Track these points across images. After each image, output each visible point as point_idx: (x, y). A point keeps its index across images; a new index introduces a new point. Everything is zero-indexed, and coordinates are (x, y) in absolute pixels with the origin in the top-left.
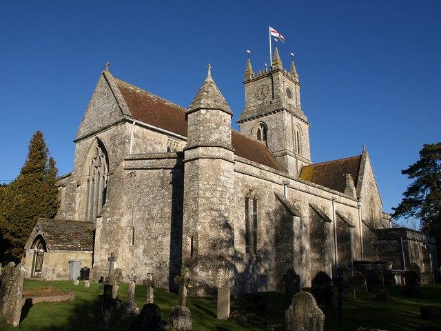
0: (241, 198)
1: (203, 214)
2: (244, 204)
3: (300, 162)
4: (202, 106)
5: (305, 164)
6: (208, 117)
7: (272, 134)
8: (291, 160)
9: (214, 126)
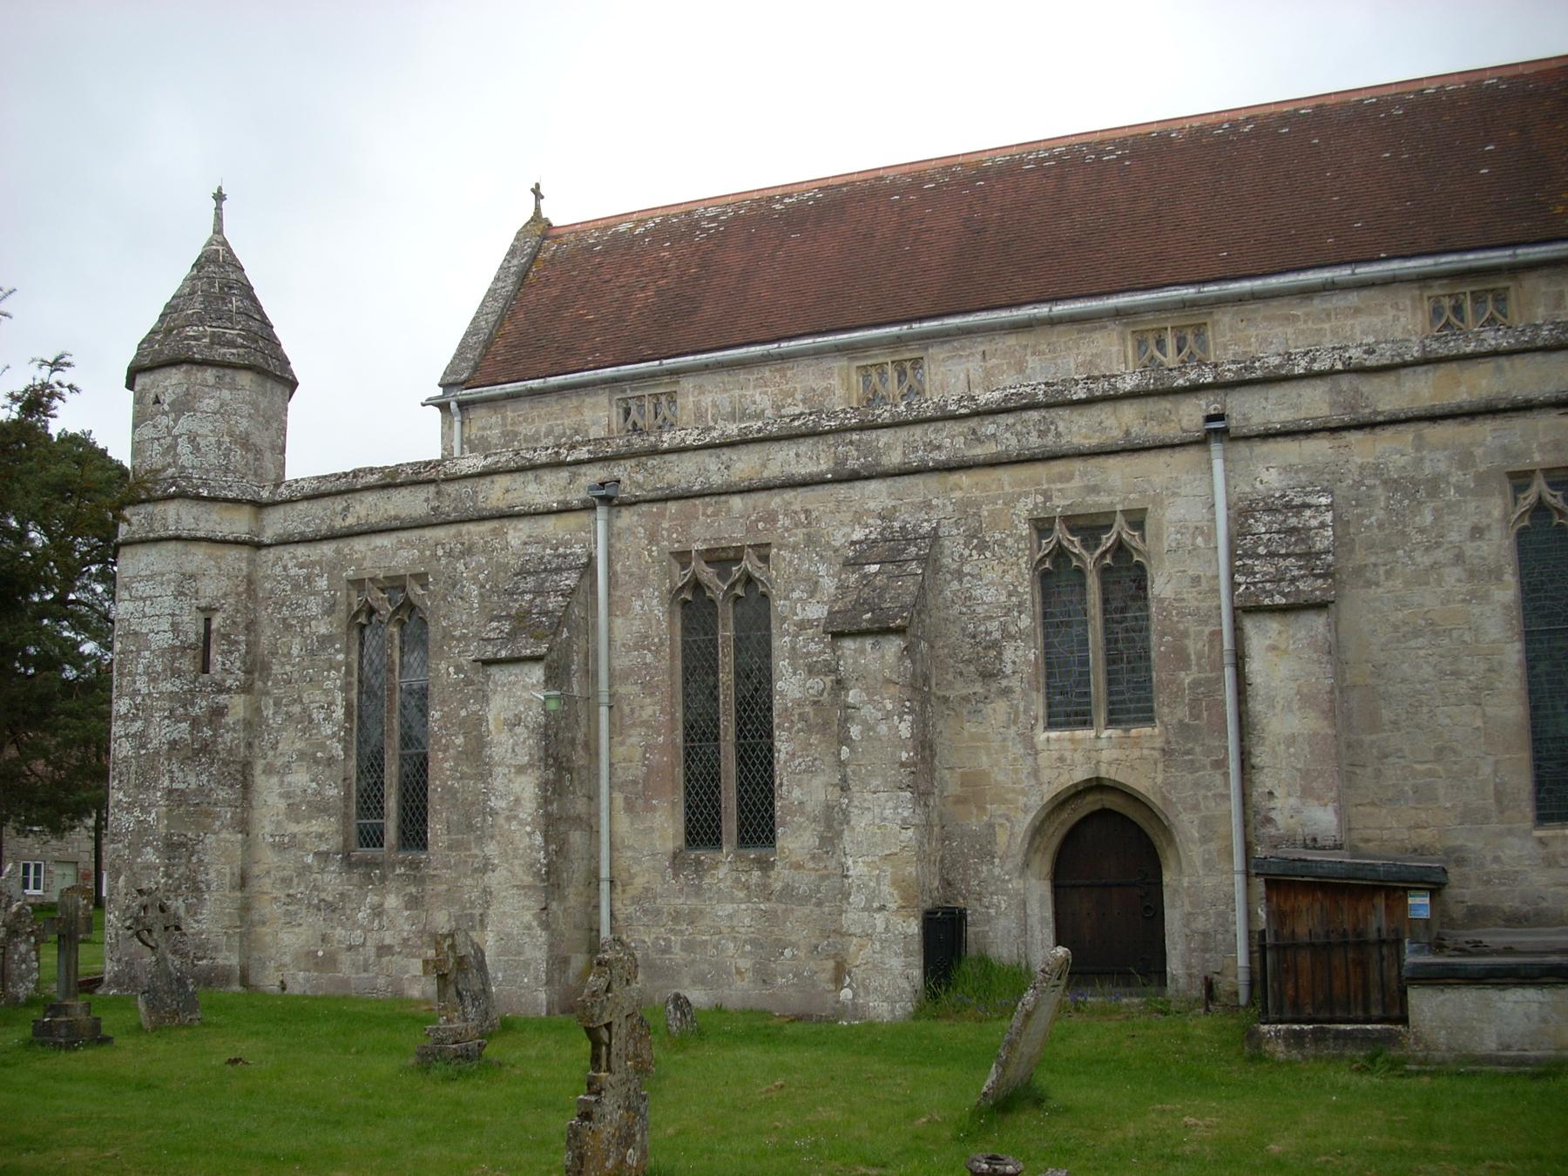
0: (325, 641)
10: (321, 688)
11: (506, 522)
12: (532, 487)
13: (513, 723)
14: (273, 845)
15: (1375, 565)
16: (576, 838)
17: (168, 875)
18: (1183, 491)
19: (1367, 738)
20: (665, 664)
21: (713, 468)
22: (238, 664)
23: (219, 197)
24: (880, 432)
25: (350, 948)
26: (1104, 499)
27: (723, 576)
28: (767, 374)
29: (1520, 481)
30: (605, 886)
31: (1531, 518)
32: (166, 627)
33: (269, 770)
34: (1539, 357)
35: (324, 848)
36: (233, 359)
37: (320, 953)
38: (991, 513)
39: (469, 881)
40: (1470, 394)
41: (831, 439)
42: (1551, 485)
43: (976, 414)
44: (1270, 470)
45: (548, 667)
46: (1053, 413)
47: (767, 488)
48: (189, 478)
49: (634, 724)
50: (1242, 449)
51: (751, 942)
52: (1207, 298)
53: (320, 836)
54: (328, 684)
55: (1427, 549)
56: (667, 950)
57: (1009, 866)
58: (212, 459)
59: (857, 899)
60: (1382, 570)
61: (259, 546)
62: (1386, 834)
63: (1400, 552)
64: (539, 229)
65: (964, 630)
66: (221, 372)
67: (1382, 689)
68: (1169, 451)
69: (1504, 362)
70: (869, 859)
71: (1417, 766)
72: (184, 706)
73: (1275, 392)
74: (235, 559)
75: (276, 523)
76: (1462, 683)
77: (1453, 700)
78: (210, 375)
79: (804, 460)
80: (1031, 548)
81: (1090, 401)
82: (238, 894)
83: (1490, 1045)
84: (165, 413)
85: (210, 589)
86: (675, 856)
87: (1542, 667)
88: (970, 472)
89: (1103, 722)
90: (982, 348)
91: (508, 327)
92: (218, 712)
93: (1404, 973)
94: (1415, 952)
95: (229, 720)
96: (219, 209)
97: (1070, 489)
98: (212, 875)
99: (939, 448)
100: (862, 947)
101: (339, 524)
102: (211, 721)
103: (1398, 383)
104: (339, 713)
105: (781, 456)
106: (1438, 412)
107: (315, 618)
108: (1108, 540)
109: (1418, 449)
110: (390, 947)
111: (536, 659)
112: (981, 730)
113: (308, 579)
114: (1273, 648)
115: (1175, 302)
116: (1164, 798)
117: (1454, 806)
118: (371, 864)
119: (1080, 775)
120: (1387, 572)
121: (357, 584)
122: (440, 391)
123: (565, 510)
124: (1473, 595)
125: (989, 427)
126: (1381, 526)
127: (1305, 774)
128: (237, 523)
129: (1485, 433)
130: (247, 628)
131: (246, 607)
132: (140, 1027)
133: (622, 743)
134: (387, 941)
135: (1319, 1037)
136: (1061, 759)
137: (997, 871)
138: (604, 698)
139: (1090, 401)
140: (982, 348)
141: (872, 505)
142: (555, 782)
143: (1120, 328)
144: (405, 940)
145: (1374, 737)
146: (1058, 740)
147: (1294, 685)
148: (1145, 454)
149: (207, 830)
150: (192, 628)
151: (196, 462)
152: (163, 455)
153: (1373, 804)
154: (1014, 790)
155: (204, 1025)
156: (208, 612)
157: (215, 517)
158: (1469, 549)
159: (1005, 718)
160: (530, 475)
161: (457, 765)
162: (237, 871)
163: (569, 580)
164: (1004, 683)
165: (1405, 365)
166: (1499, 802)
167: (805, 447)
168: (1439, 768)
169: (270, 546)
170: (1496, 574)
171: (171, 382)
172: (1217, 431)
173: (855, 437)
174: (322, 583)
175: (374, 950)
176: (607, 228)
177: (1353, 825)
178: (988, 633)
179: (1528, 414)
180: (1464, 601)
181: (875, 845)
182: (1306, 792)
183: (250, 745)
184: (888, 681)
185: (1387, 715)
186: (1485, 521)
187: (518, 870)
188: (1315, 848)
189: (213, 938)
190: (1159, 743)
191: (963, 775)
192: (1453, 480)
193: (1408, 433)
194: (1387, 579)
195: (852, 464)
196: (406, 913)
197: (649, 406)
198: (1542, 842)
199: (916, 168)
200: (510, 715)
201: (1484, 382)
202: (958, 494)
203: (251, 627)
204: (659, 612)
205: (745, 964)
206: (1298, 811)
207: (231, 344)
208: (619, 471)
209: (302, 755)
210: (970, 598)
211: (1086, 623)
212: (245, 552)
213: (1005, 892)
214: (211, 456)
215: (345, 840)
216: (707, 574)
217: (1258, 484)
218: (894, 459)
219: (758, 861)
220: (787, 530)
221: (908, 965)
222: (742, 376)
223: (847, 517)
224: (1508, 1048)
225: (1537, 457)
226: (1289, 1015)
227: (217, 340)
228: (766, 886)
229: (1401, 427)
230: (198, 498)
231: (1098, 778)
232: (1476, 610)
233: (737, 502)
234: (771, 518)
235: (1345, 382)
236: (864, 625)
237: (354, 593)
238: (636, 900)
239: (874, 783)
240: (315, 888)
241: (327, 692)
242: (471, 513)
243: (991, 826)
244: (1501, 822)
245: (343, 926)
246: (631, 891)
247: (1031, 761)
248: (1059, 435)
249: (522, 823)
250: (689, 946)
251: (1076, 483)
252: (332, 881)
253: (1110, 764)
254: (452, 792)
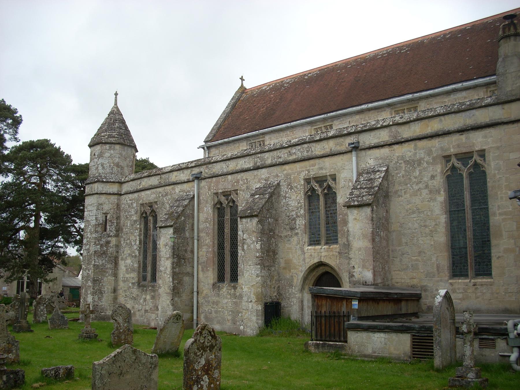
0: (135, 221)
11: (175, 186)
12: (182, 175)
13: (166, 245)
14: (122, 280)
15: (401, 190)
16: (186, 279)
17: (93, 289)
18: (346, 168)
19: (398, 248)
20: (212, 227)
21: (224, 167)
22: (114, 229)
23: (116, 94)
24: (265, 153)
25: (139, 311)
26: (324, 171)
27: (465, 165)
28: (289, 133)
29: (448, 159)
30: (195, 294)
31: (451, 171)
32: (94, 219)
33: (122, 259)
34: (453, 115)
35: (134, 281)
36: (114, 142)
38: (294, 177)
40: (431, 130)
41: (253, 157)
42: (458, 160)
43: (290, 146)
44: (371, 159)
45: (175, 229)
46: (311, 144)
47: (237, 172)
48: (101, 176)
49: (204, 245)
50: (363, 152)
51: (231, 311)
52: (417, 98)
53: (133, 278)
54: (135, 234)
55: (417, 184)
56: (211, 313)
57: (297, 289)
58: (108, 170)
59: (245, 299)
60: (403, 191)
61: (121, 195)
62: (403, 281)
63: (409, 185)
64: (242, 90)
65: (286, 214)
66: (111, 145)
67: (402, 232)
68: (342, 155)
69: (442, 118)
70: (248, 286)
71: (413, 258)
72: (99, 241)
73: (373, 133)
74: (114, 199)
75: (126, 188)
76: (427, 229)
77: (424, 235)
78: (107, 146)
79: (246, 163)
80: (304, 188)
81: (321, 140)
82: (113, 294)
83: (369, 351)
84: (96, 158)
85: (106, 208)
86: (213, 285)
87: (455, 223)
88: (288, 165)
89: (323, 243)
90: (349, 120)
91: (226, 122)
92: (108, 242)
93: (345, 327)
94: (353, 319)
95: (111, 245)
96: (116, 98)
97: (315, 169)
98: (106, 289)
99: (280, 157)
100: (246, 313)
101: (139, 188)
102: (106, 245)
103: (409, 128)
104: (138, 243)
105: (241, 163)
106: (420, 137)
107: (133, 215)
108: (325, 184)
109: (415, 150)
110: (147, 310)
111: (171, 226)
112: (290, 246)
113: (132, 204)
114: (355, 219)
115: (405, 100)
116: (339, 268)
117: (424, 272)
118: (144, 286)
119: (316, 260)
120: (405, 192)
121: (142, 205)
122: (204, 144)
123: (188, 181)
124: (431, 199)
125: (293, 150)
126: (403, 177)
127: (363, 260)
128: (114, 188)
129: (436, 143)
130: (117, 218)
131: (117, 212)
132: (49, 329)
133: (201, 251)
135: (323, 346)
136: (311, 255)
137: (293, 291)
138: (196, 237)
139: (321, 140)
140: (349, 120)
141: (263, 176)
142: (177, 262)
143: (390, 110)
144: (151, 308)
145: (399, 248)
146: (310, 249)
147: (361, 231)
148: (336, 156)
149: (104, 276)
150: (101, 218)
151: (103, 172)
152: (95, 170)
153: (399, 270)
154: (298, 265)
155: (69, 329)
156: (106, 214)
157: (108, 187)
158: (430, 183)
159: (296, 242)
160: (181, 171)
162: (113, 288)
163: (186, 203)
164: (296, 231)
165: (411, 121)
166: (438, 270)
167: (247, 159)
168: (419, 258)
169: (123, 195)
170: (438, 192)
171: (98, 148)
172: (356, 148)
173: (259, 155)
174: (135, 205)
176: (260, 88)
177: (393, 277)
178: (292, 216)
179: (450, 135)
180: (428, 201)
181: (250, 282)
182: (364, 267)
183: (117, 252)
184: (254, 231)
185: (404, 240)
186: (435, 173)
187: (166, 288)
188: (366, 285)
189: (106, 307)
190: (338, 250)
191: (285, 260)
192: (425, 160)
193: (412, 144)
194: (405, 194)
195: (258, 164)
197: (258, 145)
198: (451, 284)
199: (347, 60)
200: (165, 243)
201: (436, 125)
202: (285, 172)
203: (118, 218)
204: (211, 211)
205: (229, 318)
206: (361, 273)
207: (114, 137)
208: (202, 169)
209: (129, 255)
210: (288, 205)
211: (319, 212)
212: (116, 197)
213: (296, 297)
214: (108, 170)
215: (139, 279)
216: (458, 164)
217: (367, 165)
218: (269, 162)
219: (233, 287)
220: (242, 185)
221: (257, 319)
222: (282, 134)
223: (257, 180)
224: (375, 352)
225: (452, 150)
226: (324, 339)
227: (110, 136)
228: (235, 294)
229: (410, 143)
230: (103, 182)
231: (321, 262)
232: (432, 204)
233: (229, 177)
234: (238, 182)
235: (394, 129)
236: (247, 214)
237: (142, 208)
238: (204, 298)
239: (250, 263)
240: (132, 293)
241: (135, 236)
242: (168, 184)
243: (292, 276)
244: (438, 277)
245: (137, 304)
246: (203, 295)
247: (301, 255)
248: (312, 151)
249: (167, 275)
250: (216, 312)
251: (317, 167)
252: (135, 291)
253: (324, 257)
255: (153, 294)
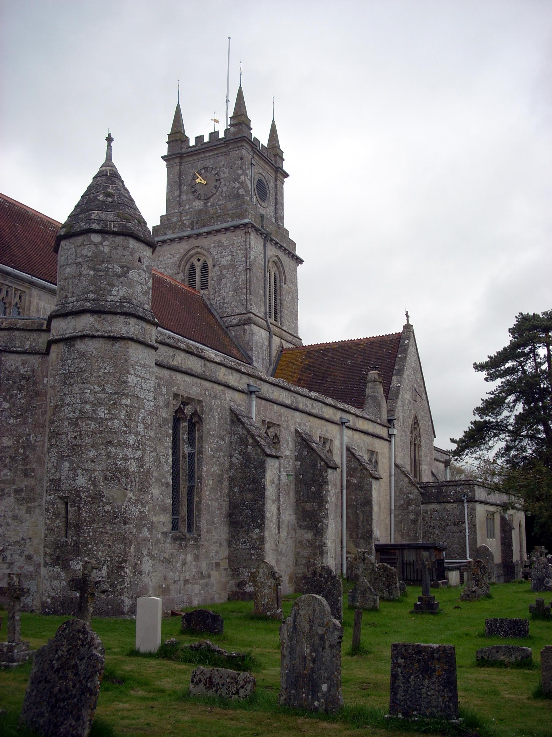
0: (165, 420)
1: (92, 453)
2: (171, 431)
3: (276, 341)
4: (95, 226)
5: (286, 345)
6: (106, 250)
7: (221, 277)
8: (259, 335)
9: (118, 270)
10: (163, 446)
35: (165, 530)
37: (164, 586)
39: (212, 548)
96: (109, 147)
110: (188, 580)
134: (187, 578)
161: (210, 493)
175: (183, 582)
196: (194, 563)
241: (166, 448)
245: (171, 570)
252: (168, 547)
254: (208, 505)
255: (196, 552)
